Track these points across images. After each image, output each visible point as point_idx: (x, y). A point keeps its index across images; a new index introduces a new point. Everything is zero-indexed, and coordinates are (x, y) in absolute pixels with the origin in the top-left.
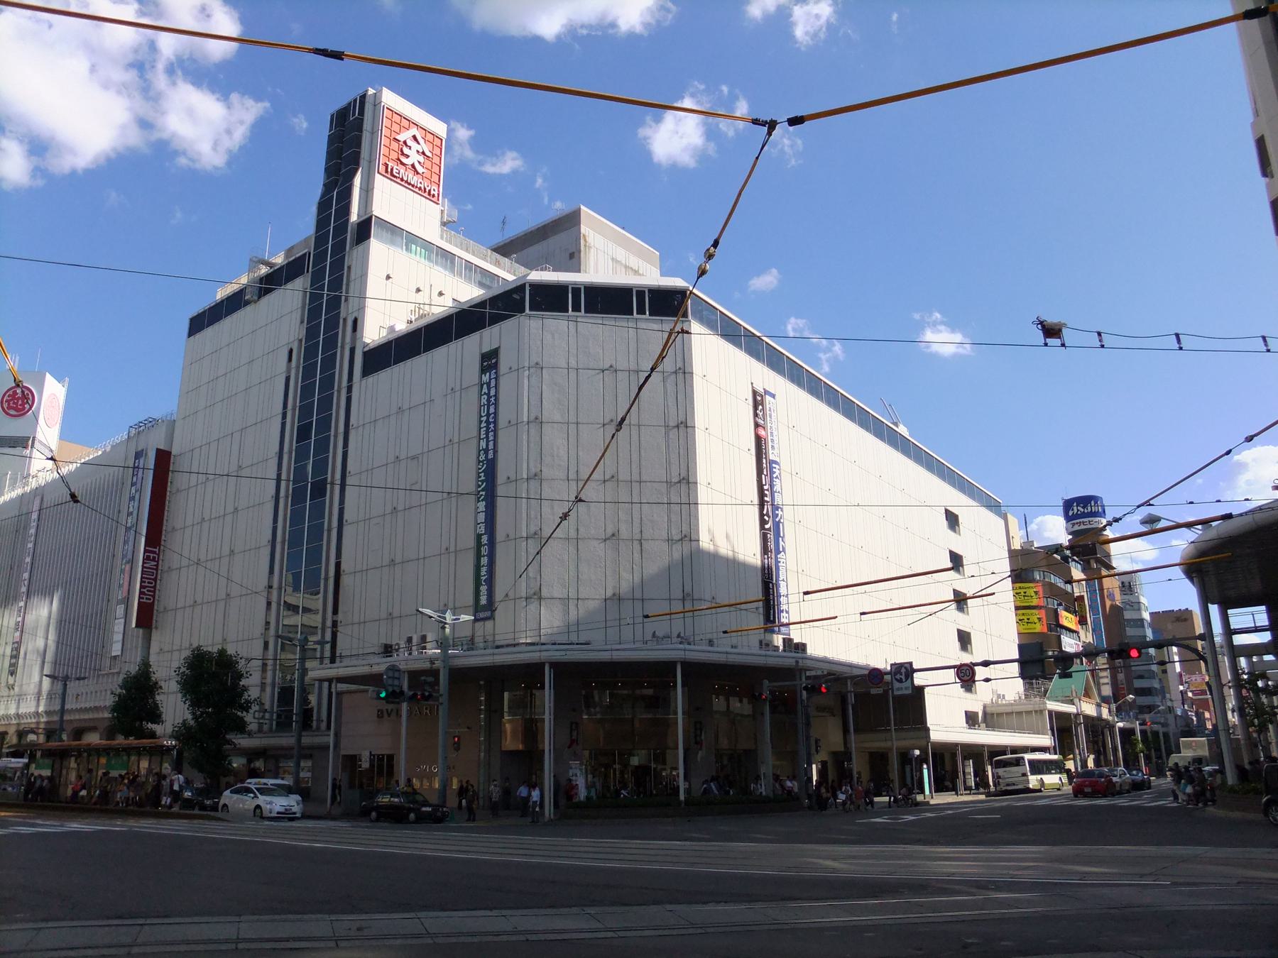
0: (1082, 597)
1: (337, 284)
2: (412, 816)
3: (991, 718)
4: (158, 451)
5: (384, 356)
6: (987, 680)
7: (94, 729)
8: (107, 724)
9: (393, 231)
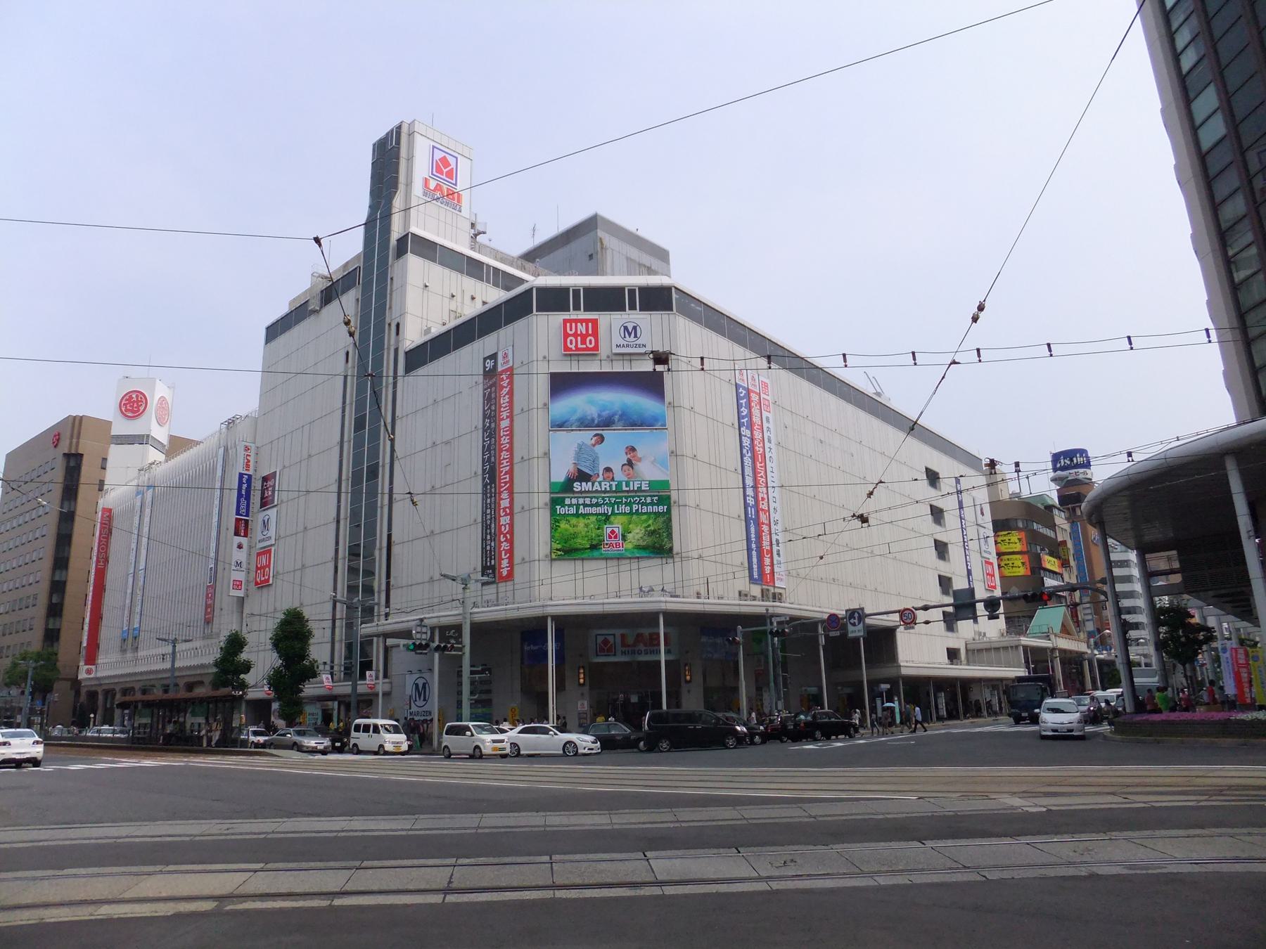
0: (1064, 542)
1: (382, 295)
3: (977, 652)
5: (419, 357)
6: (927, 622)
7: (201, 683)
8: (211, 678)
9: (427, 249)
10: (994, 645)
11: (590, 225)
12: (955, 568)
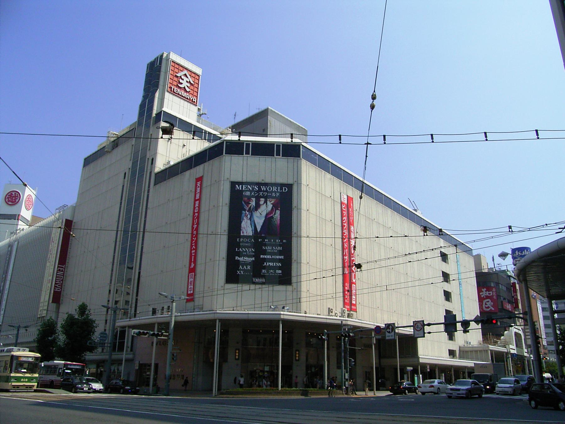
2: (122, 390)
3: (464, 353)
4: (66, 220)
6: (429, 333)
10: (474, 349)
11: (263, 114)
12: (454, 307)
